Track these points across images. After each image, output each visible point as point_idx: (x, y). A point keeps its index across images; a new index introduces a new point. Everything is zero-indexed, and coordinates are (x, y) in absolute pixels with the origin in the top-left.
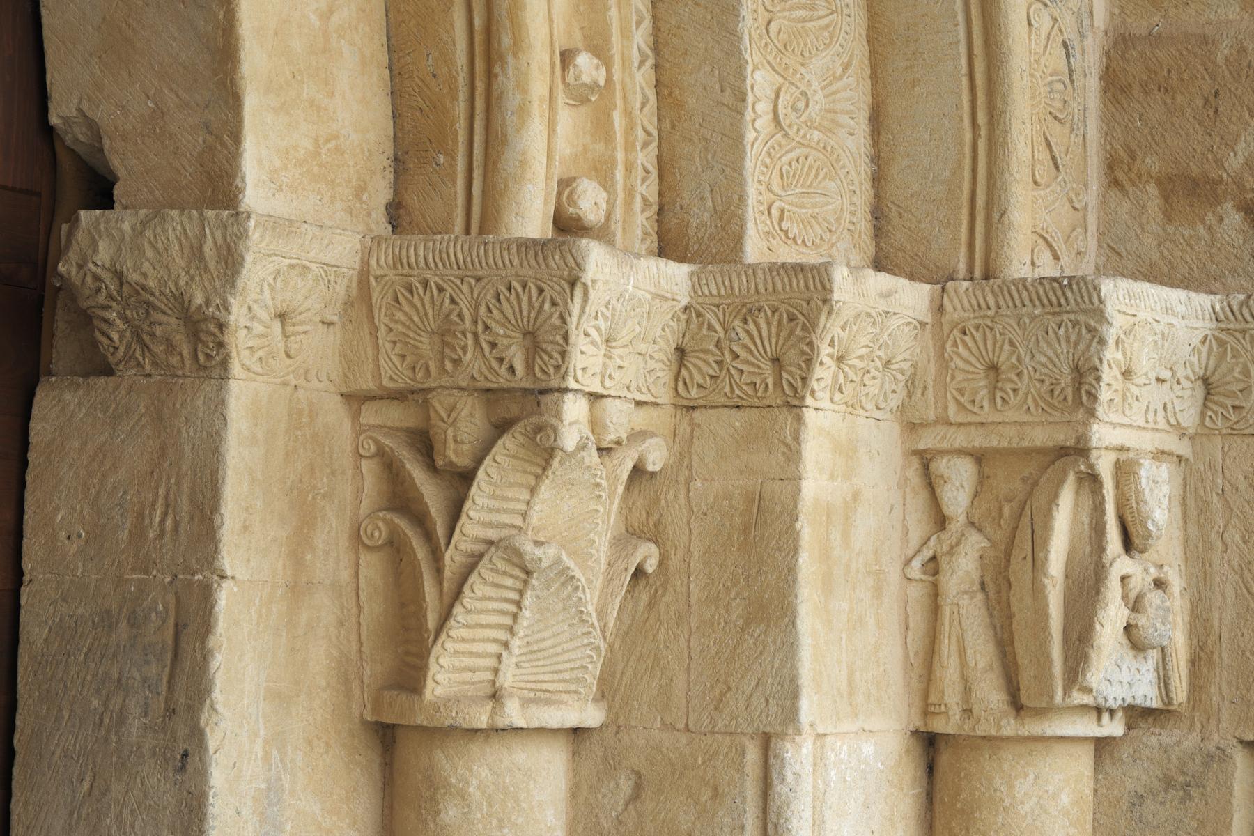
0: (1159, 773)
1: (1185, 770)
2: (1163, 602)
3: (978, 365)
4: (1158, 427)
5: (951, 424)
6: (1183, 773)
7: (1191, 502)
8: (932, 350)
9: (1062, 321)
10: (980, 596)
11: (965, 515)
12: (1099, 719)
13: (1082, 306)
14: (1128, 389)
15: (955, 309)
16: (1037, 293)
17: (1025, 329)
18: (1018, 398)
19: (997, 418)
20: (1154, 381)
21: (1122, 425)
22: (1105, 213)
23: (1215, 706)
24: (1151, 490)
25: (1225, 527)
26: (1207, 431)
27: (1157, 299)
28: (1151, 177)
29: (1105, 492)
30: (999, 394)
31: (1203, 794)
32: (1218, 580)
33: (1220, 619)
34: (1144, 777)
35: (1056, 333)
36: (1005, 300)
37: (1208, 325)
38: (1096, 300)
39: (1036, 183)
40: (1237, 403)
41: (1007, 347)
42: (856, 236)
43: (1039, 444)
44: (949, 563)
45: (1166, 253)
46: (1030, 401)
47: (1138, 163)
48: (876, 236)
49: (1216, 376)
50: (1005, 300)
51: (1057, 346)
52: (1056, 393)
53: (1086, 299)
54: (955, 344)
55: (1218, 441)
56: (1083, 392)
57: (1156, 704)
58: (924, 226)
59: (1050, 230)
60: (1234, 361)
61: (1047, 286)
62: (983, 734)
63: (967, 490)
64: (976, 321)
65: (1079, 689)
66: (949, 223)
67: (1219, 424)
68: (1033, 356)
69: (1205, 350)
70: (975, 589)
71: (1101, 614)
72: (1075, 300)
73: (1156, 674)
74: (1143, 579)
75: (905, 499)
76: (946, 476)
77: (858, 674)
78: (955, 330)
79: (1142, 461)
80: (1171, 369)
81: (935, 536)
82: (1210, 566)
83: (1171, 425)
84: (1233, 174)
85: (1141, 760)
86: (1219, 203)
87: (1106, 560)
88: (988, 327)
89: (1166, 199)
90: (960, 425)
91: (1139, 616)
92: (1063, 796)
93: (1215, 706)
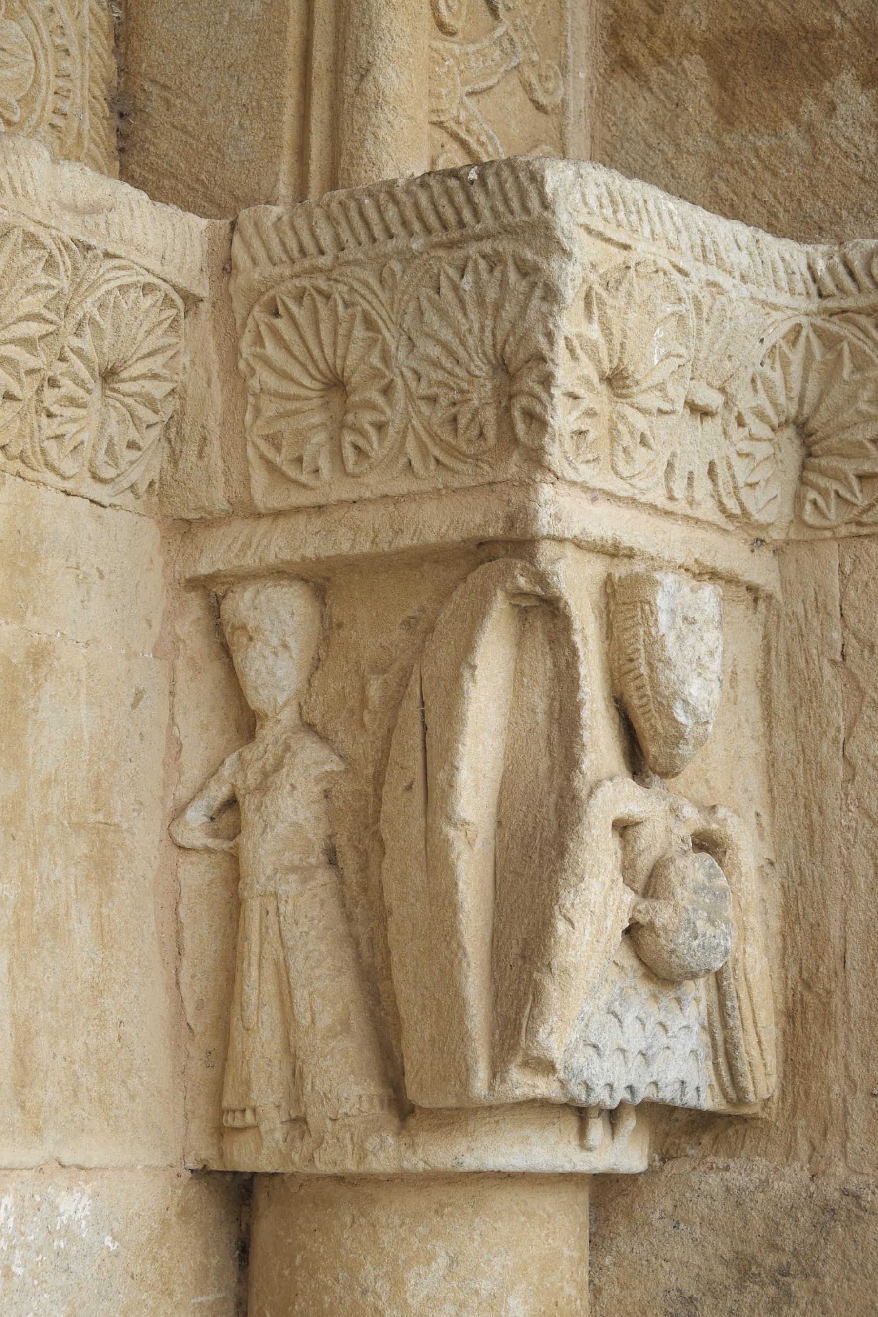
0: (724, 1250)
1: (779, 1241)
2: (710, 876)
3: (306, 381)
4: (699, 513)
5: (260, 516)
6: (774, 1247)
7: (780, 685)
8: (214, 357)
9: (468, 258)
10: (324, 876)
11: (294, 706)
12: (583, 1132)
13: (508, 219)
14: (622, 417)
15: (254, 262)
16: (416, 206)
17: (393, 288)
18: (387, 444)
19: (347, 490)
20: (680, 406)
21: (611, 497)
22: (603, 124)
23: (837, 1105)
24: (680, 638)
25: (850, 729)
26: (808, 535)
27: (679, 223)
28: (693, 42)
29: (577, 638)
30: (348, 438)
31: (816, 1292)
32: (837, 840)
33: (845, 922)
34: (697, 1260)
35: (455, 288)
36: (352, 229)
37: (802, 303)
38: (534, 204)
39: (441, 26)
40: (867, 467)
41: (359, 332)
42: (70, 141)
43: (432, 539)
44: (258, 809)
45: (723, 188)
46: (411, 447)
47: (667, 17)
48: (121, 150)
49: (823, 415)
50: (352, 229)
51: (460, 316)
52: (463, 421)
53: (515, 204)
54: (259, 340)
55: (831, 553)
56: (517, 414)
57: (709, 1101)
58: (211, 120)
59: (474, 126)
60: (857, 376)
61: (437, 188)
62: (331, 1170)
63: (295, 652)
64: (296, 282)
65: (525, 1064)
66: (260, 107)
67: (832, 515)
68: (412, 345)
69: (796, 357)
70: (313, 861)
71: (567, 898)
72: (493, 209)
73: (706, 1038)
74: (669, 830)
75: (173, 681)
76: (250, 626)
77: (43, 1041)
78: (257, 308)
79: (658, 576)
80: (722, 390)
81: (234, 756)
82: (821, 811)
83: (730, 516)
84: (853, 15)
85: (688, 1222)
86: (827, 76)
87: (581, 785)
88: (320, 292)
89: (722, 81)
90: (278, 514)
91: (657, 905)
92: (512, 1302)
93: (837, 1105)
